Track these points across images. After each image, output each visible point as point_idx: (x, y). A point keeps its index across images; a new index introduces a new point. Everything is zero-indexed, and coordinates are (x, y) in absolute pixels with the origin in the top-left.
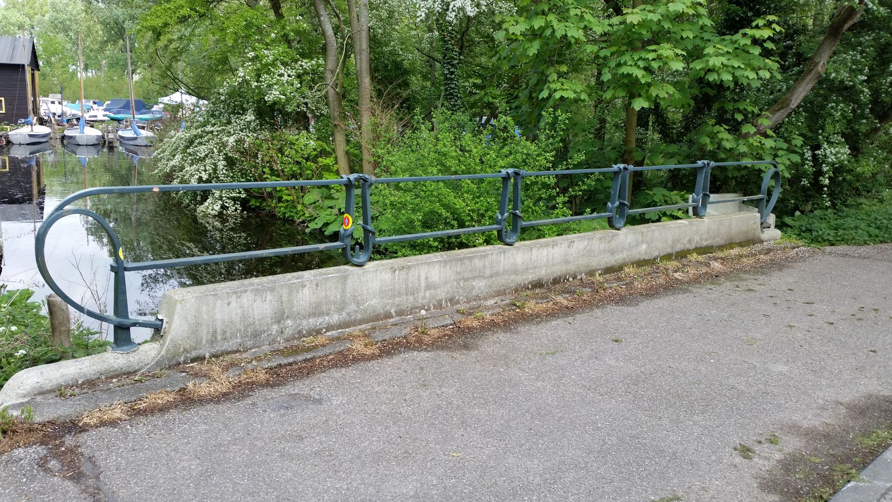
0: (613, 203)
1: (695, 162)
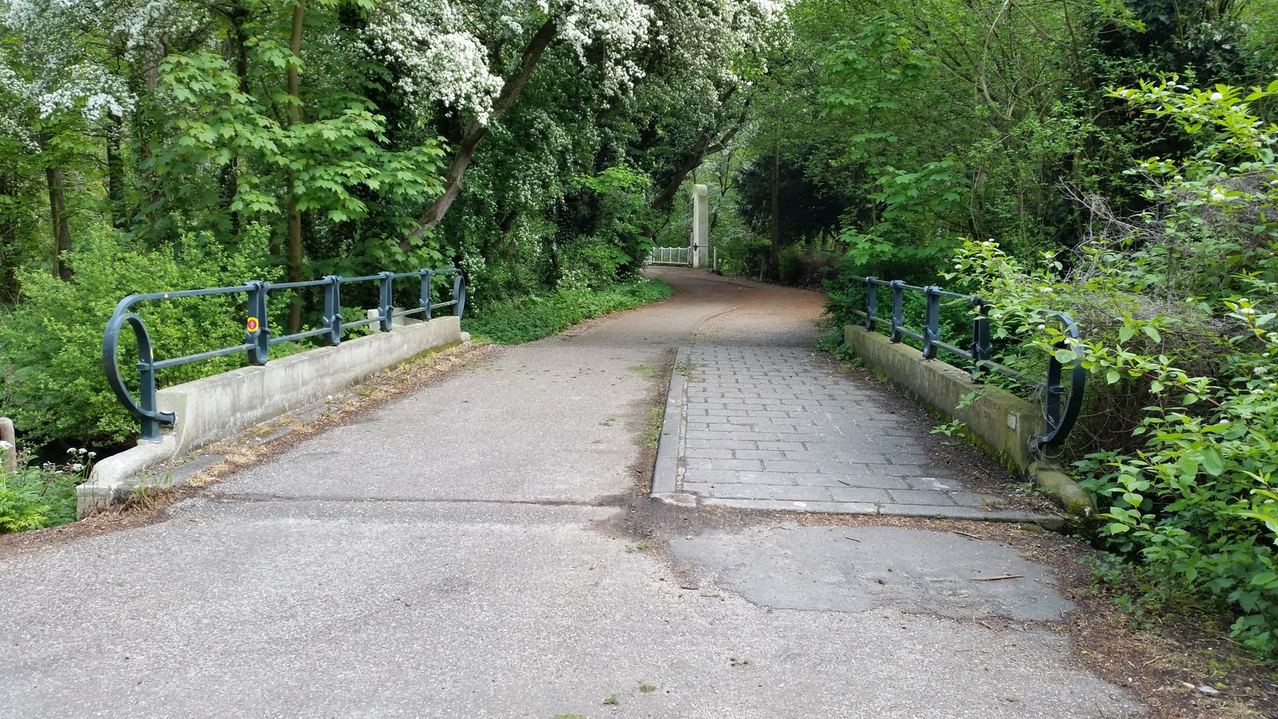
0: (329, 318)
1: (321, 279)
